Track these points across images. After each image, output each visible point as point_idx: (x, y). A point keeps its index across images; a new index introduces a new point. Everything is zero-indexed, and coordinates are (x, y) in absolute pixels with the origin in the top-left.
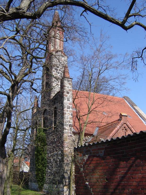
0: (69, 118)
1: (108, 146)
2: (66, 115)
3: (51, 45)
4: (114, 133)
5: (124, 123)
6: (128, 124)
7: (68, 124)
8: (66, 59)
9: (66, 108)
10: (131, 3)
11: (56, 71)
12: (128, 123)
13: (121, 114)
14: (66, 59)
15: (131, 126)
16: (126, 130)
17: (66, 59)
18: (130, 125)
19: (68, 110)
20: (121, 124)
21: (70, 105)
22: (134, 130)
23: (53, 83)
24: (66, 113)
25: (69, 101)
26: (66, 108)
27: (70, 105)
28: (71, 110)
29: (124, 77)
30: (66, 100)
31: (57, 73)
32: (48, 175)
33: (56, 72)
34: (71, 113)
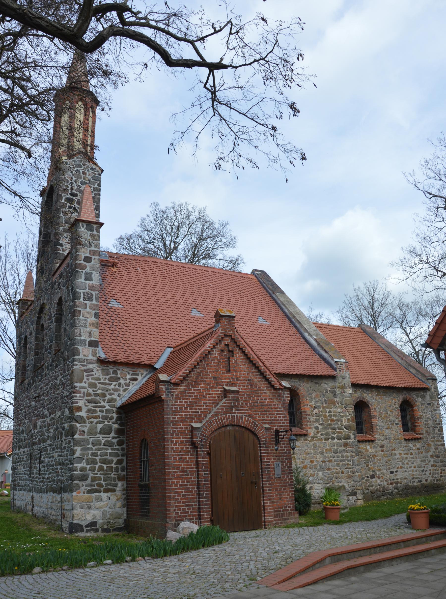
0: (88, 324)
1: (93, 408)
2: (81, 317)
3: (75, 139)
4: (195, 361)
5: (226, 336)
6: (236, 337)
7: (85, 341)
8: (97, 173)
9: (82, 300)
10: (151, 49)
11: (68, 204)
12: (236, 333)
13: (217, 311)
14: (97, 173)
15: (244, 343)
16: (229, 351)
17: (97, 175)
18: (242, 341)
19: (86, 304)
20: (216, 336)
21: (91, 292)
22: (251, 352)
23: (60, 236)
24: (80, 311)
25: (91, 280)
26: (82, 300)
27: (91, 292)
28: (94, 304)
29: (29, 255)
30: (81, 279)
31: (71, 210)
32: (389, 412)
33: (70, 207)
34: (94, 312)
